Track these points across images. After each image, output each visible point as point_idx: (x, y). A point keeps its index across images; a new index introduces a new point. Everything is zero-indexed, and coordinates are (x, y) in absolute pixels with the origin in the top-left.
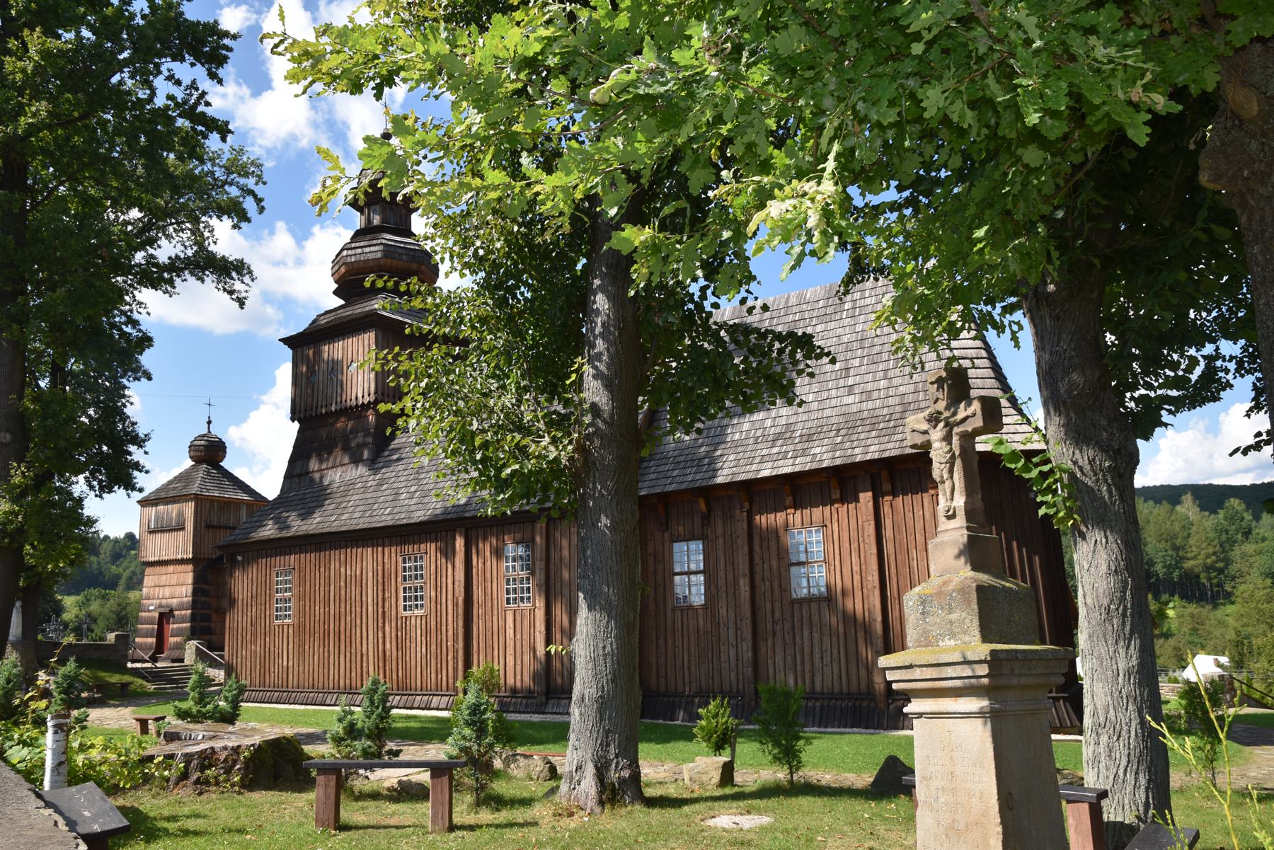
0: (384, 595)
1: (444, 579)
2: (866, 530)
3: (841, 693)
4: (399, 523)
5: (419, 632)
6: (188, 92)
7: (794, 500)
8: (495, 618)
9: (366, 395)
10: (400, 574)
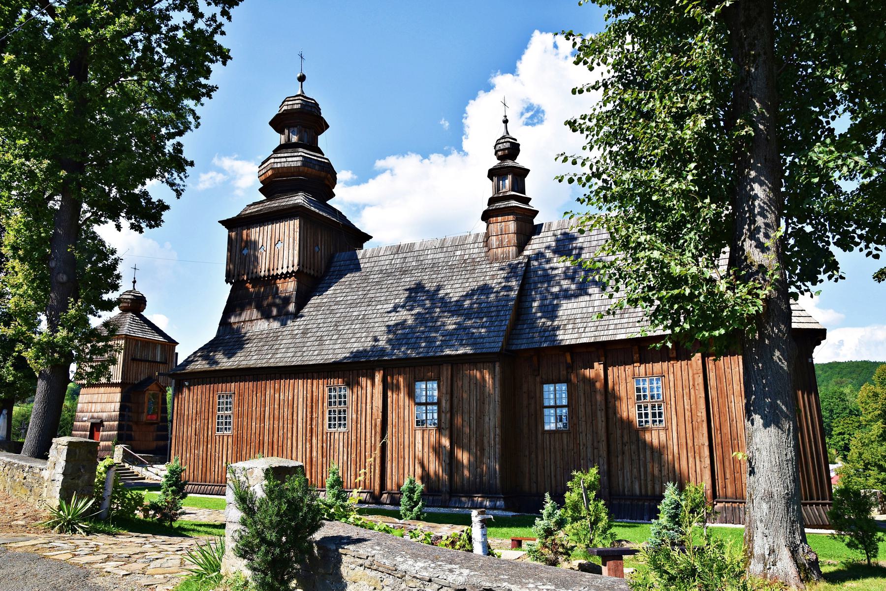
0: (312, 415)
1: (364, 405)
2: (696, 380)
3: (647, 495)
4: (328, 362)
5: (341, 444)
6: (208, 23)
7: (640, 357)
8: (406, 436)
9: (290, 266)
10: (326, 401)
